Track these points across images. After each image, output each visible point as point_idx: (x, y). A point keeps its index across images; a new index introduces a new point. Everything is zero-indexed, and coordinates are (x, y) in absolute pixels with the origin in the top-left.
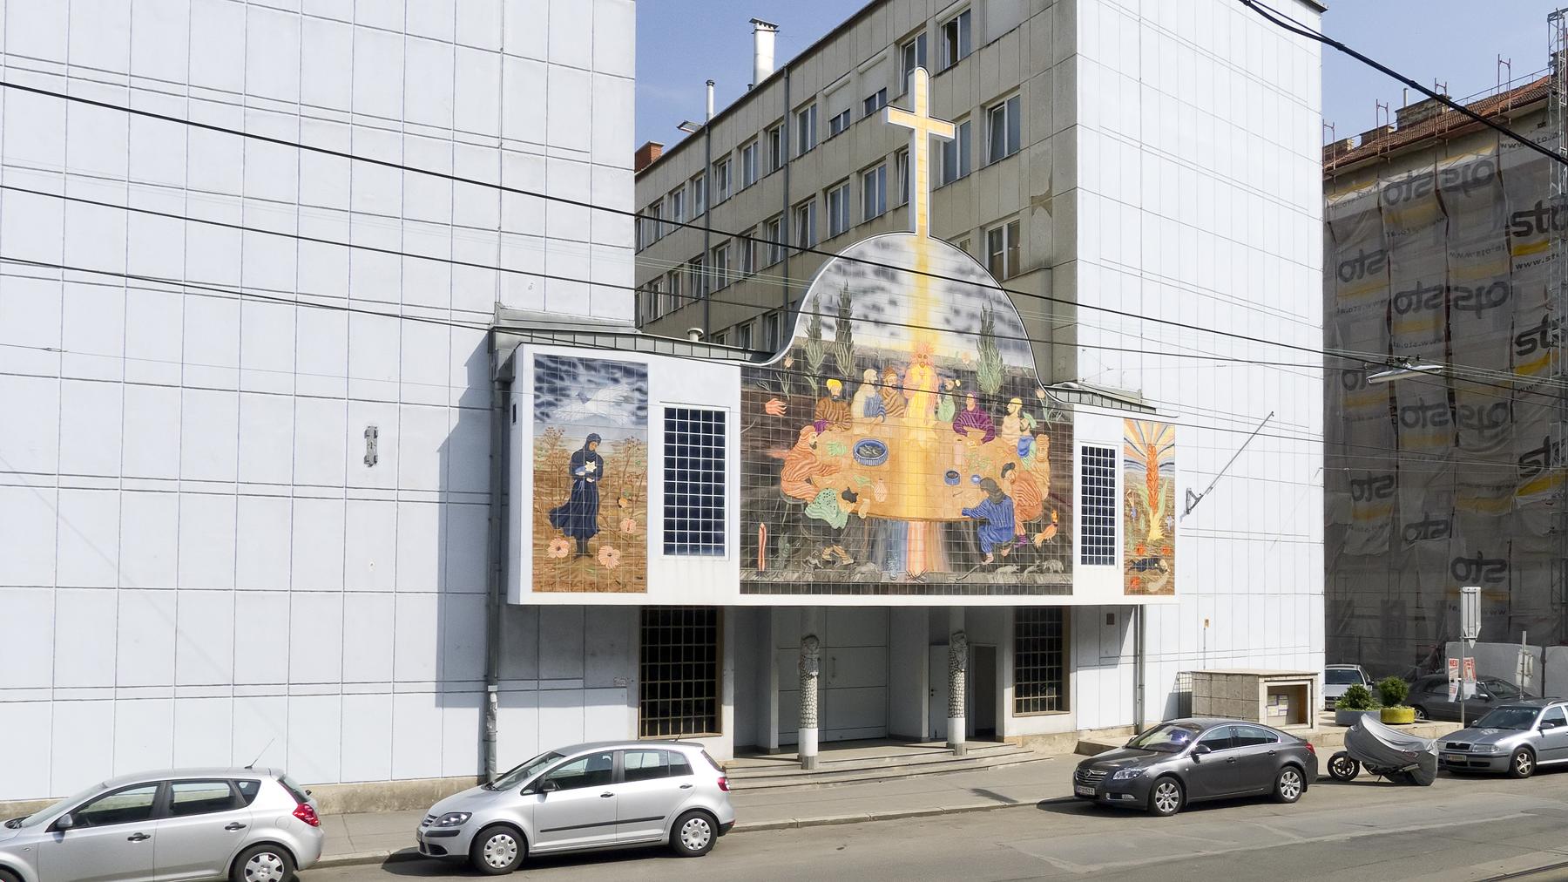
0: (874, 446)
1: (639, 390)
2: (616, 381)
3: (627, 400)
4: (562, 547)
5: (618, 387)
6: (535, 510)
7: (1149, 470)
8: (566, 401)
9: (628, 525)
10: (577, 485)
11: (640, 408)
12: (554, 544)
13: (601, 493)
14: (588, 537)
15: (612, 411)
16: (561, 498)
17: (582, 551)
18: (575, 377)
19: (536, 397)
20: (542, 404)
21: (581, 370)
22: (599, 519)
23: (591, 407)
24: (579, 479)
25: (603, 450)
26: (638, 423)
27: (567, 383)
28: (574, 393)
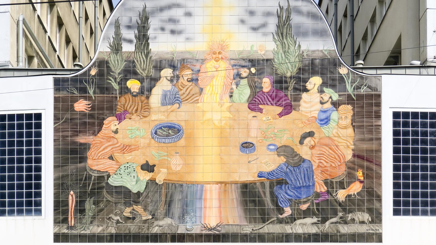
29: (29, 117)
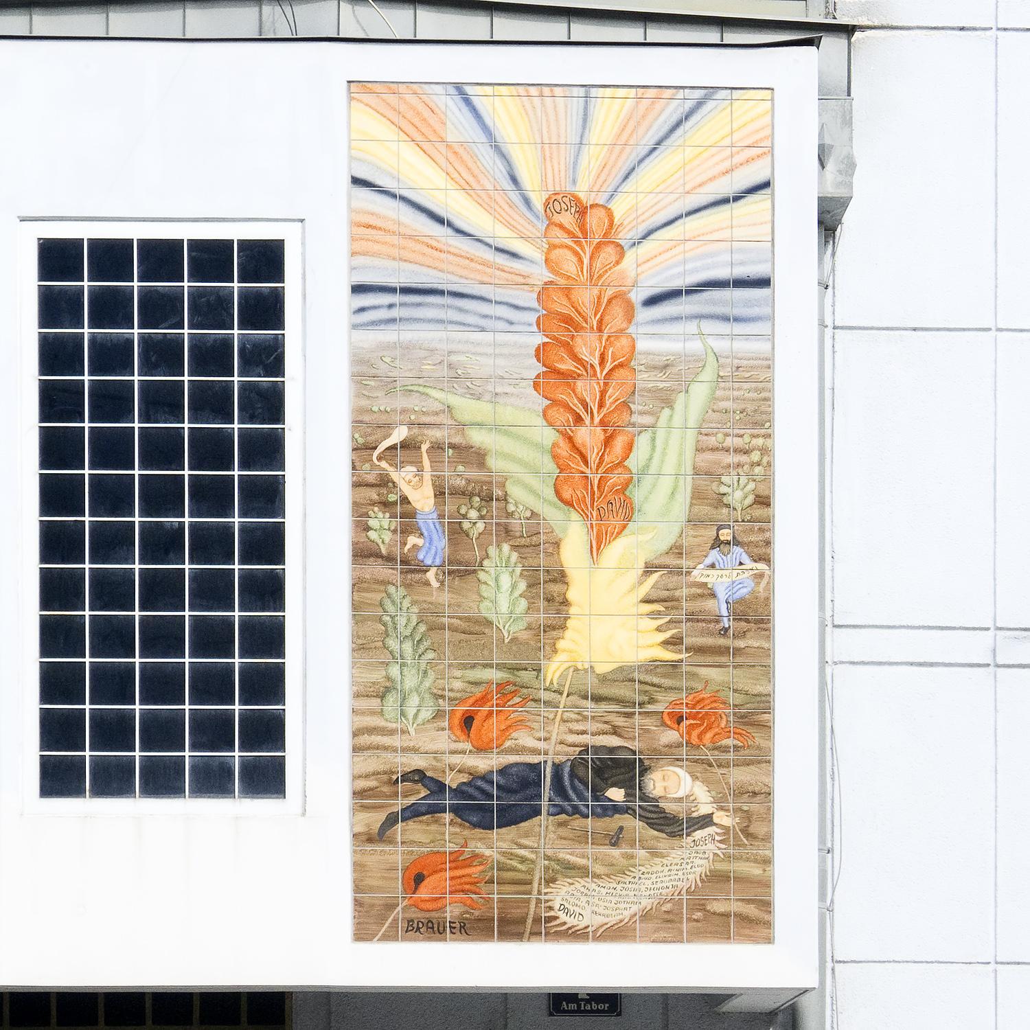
7: (561, 325)
29: (212, 257)
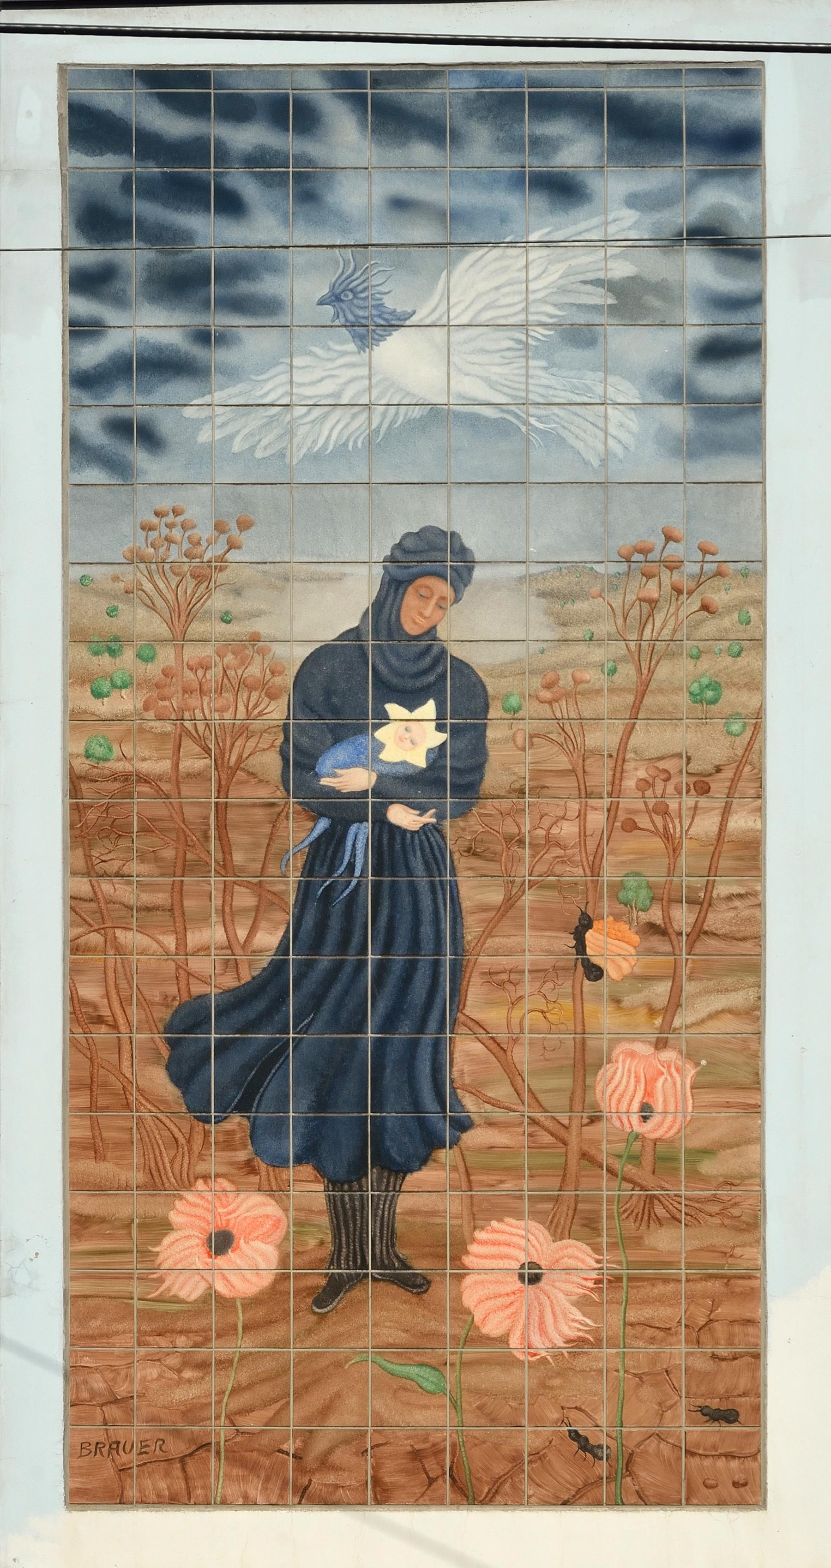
0: (243, 1464)
1: (713, 236)
2: (563, 189)
3: (630, 301)
4: (239, 1231)
5: (580, 223)
6: (81, 1015)
8: (255, 342)
9: (642, 1087)
10: (325, 852)
11: (714, 352)
12: (190, 1215)
13: (476, 891)
14: (396, 1169)
15: (545, 382)
16: (237, 936)
17: (364, 1257)
18: (307, 188)
19: (79, 330)
20: (118, 370)
21: (346, 138)
22: (466, 1054)
23: (408, 364)
24: (341, 811)
25: (483, 627)
26: (693, 448)
27: (263, 225)
28: (304, 287)
